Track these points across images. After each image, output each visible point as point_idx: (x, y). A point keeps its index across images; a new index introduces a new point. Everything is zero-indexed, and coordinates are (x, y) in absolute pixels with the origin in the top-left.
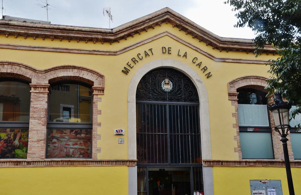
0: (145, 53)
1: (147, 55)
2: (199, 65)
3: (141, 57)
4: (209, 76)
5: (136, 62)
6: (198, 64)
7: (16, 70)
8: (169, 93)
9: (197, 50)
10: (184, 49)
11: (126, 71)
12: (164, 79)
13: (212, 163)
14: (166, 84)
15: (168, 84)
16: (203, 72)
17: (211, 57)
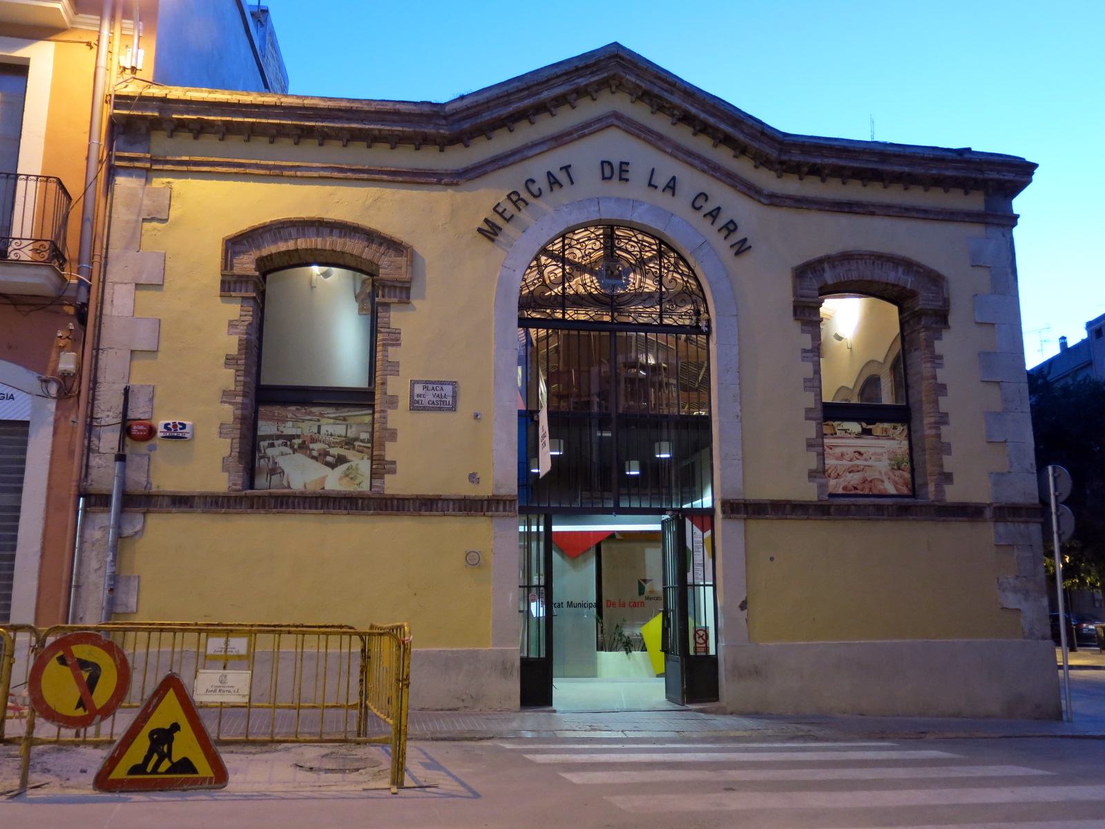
0: (549, 180)
1: (553, 181)
2: (714, 215)
4: (741, 248)
9: (713, 170)
10: (668, 167)
11: (491, 231)
13: (854, 469)
17: (751, 191)
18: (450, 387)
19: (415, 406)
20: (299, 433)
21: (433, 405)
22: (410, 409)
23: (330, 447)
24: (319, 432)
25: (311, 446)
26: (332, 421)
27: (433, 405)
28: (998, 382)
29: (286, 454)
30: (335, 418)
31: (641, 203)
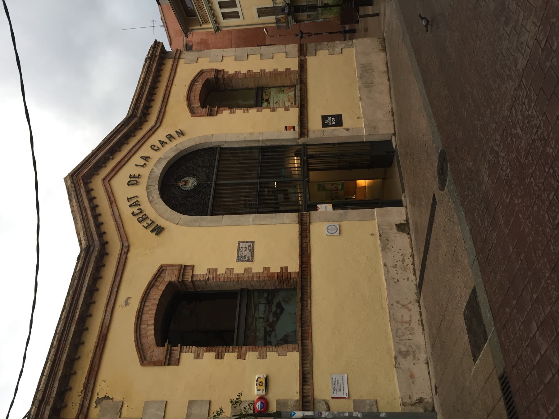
6: (161, 144)
10: (137, 159)
14: (185, 185)
17: (153, 130)
18: (241, 244)
19: (251, 259)
20: (263, 328)
21: (251, 251)
22: (253, 261)
23: (272, 311)
24: (262, 318)
25: (271, 321)
26: (257, 312)
27: (251, 251)
28: (248, 55)
29: (275, 334)
30: (255, 310)
31: (153, 169)
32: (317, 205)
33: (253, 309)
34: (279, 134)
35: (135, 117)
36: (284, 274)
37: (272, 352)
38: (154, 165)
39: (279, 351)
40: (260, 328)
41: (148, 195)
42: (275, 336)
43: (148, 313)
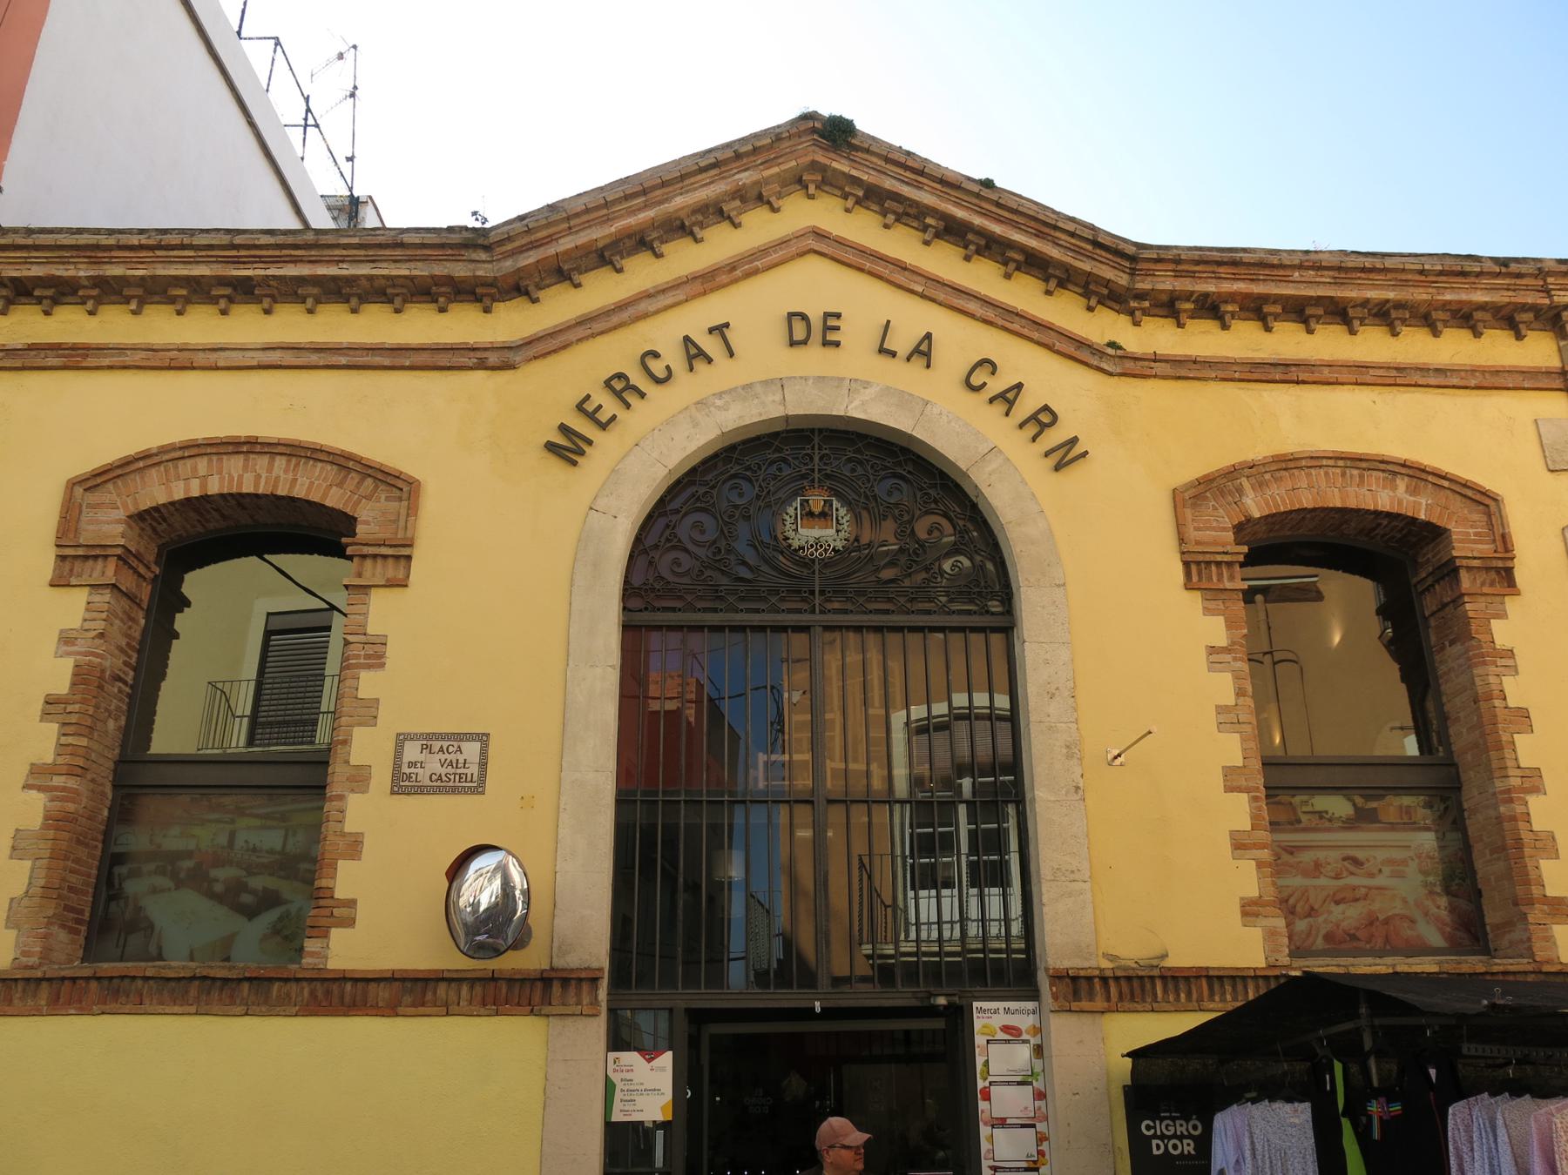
1: (694, 354)
2: (1008, 398)
3: (657, 367)
5: (631, 398)
7: (309, 484)
8: (826, 564)
11: (573, 447)
12: (800, 491)
14: (811, 514)
15: (824, 515)
16: (1034, 440)
18: (477, 746)
21: (439, 783)
22: (393, 793)
27: (439, 783)
29: (163, 891)
32: (669, 1055)
33: (269, 810)
34: (1072, 877)
35: (1133, 273)
36: (326, 912)
37: (30, 878)
38: (888, 388)
39: (26, 902)
40: (194, 836)
41: (740, 390)
42: (155, 890)
43: (245, 468)
